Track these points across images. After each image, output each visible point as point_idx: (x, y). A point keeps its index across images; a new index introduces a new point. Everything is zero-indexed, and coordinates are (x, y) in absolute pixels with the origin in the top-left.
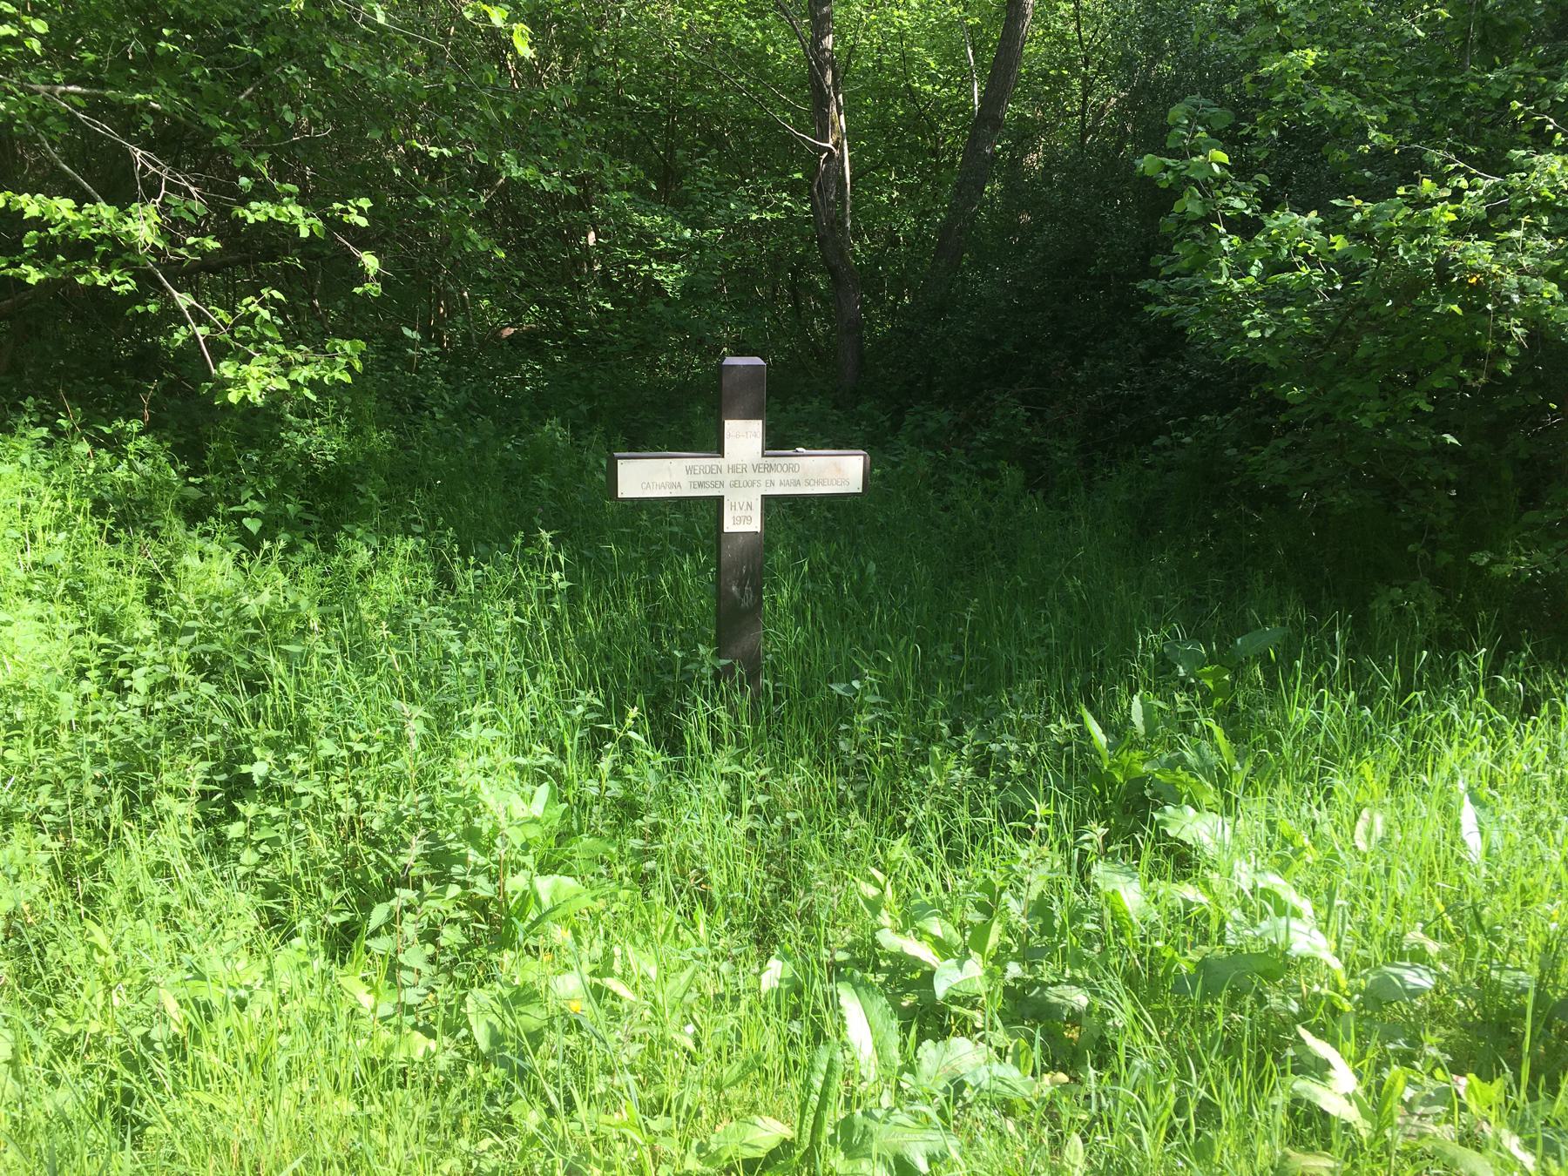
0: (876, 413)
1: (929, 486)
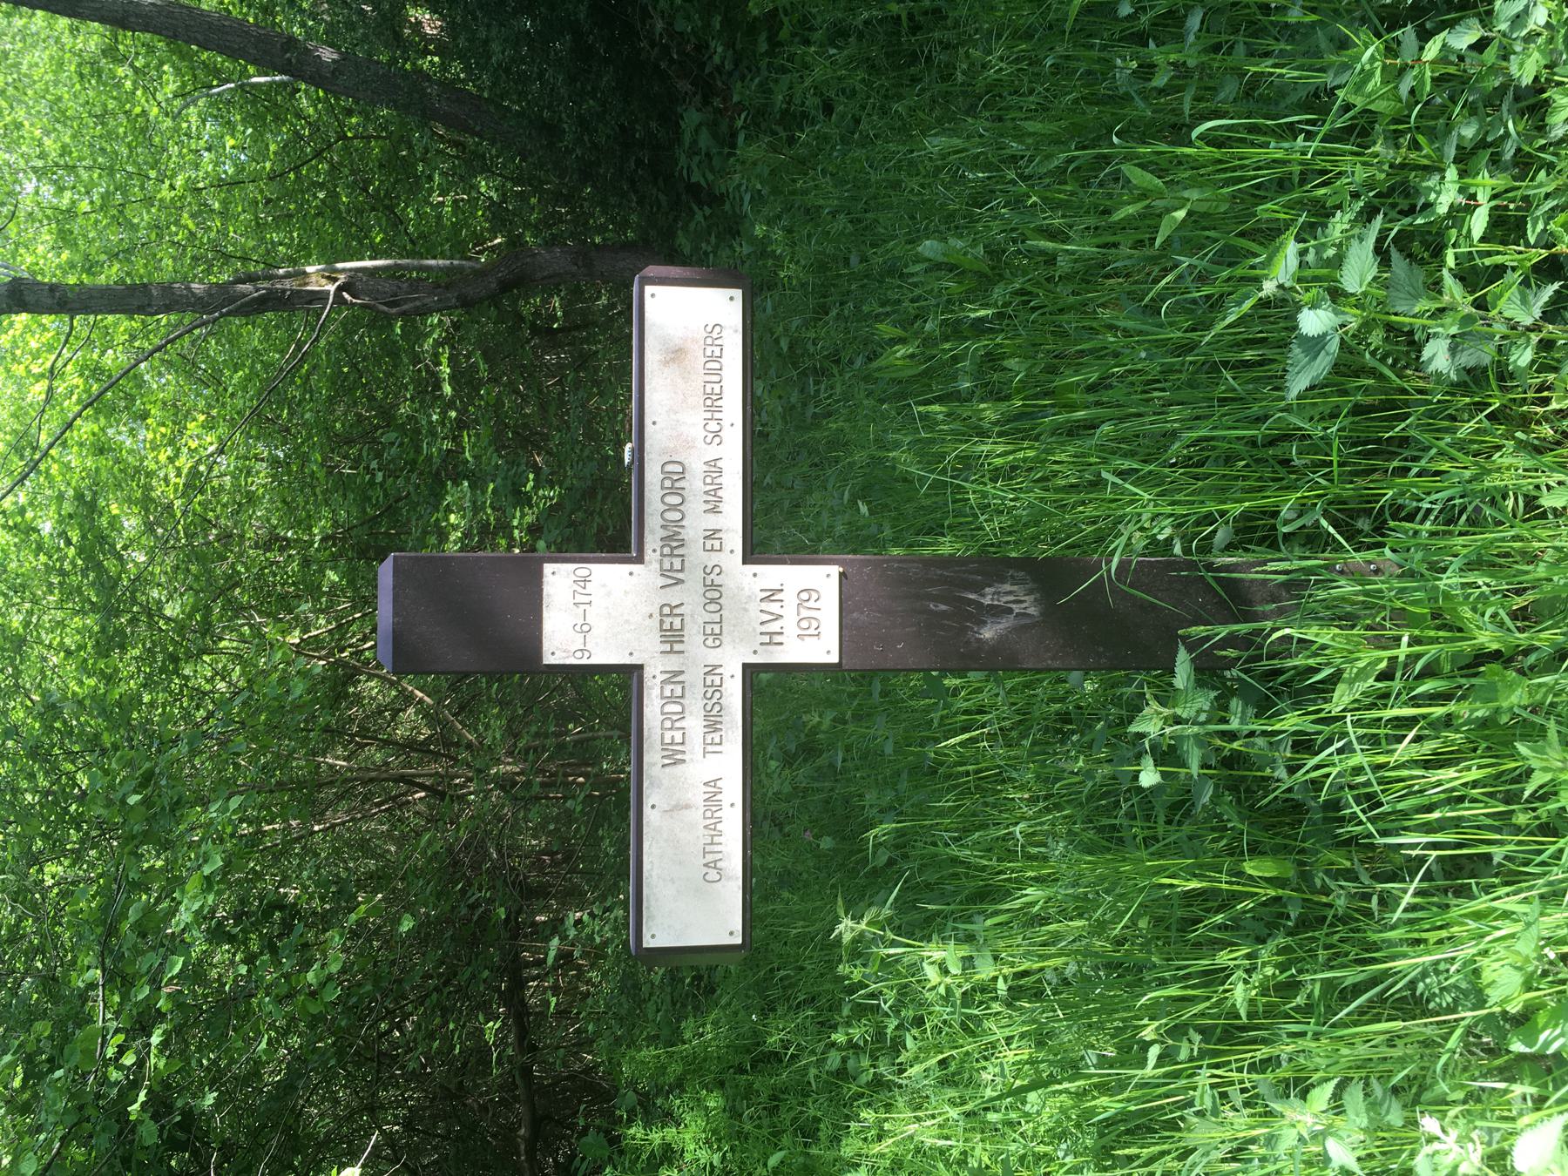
0: (692, 226)
1: (792, 141)
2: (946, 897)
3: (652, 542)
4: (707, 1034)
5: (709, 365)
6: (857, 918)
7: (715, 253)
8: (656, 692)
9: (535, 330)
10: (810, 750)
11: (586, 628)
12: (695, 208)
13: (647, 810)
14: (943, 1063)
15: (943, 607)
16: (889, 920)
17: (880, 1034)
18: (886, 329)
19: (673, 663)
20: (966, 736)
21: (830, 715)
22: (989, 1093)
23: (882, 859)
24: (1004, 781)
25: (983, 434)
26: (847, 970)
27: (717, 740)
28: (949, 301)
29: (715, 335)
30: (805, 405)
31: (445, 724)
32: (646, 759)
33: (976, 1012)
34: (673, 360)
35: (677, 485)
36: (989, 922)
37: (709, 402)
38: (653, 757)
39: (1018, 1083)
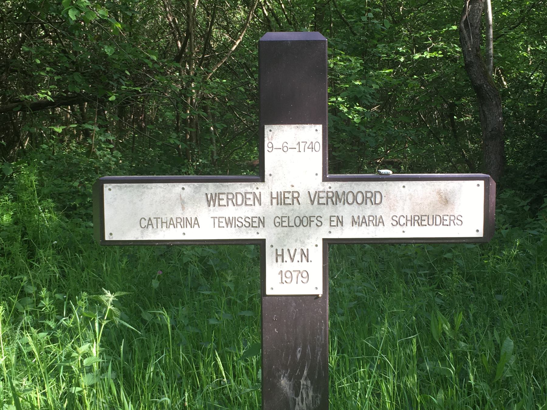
0: (517, 199)
2: (125, 353)
3: (335, 186)
4: (46, 216)
5: (438, 218)
6: (114, 304)
7: (501, 213)
8: (249, 189)
9: (452, 106)
10: (208, 272)
11: (285, 149)
12: (529, 201)
13: (181, 185)
14: (31, 355)
15: (299, 356)
16: (112, 322)
17: (45, 317)
18: (459, 319)
19: (266, 199)
20: (221, 367)
21: (232, 286)
22: (15, 382)
23: (146, 316)
24: (193, 390)
25: (399, 377)
26: (84, 298)
27: (221, 225)
28: (477, 356)
29: (456, 221)
30: (412, 267)
31: (221, 57)
32: (210, 184)
33: (61, 374)
34: (441, 197)
35: (368, 200)
36: (112, 382)
37: (417, 218)
38: (211, 188)
39: (21, 399)
